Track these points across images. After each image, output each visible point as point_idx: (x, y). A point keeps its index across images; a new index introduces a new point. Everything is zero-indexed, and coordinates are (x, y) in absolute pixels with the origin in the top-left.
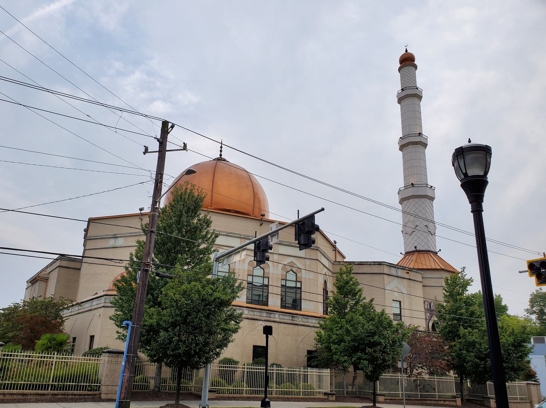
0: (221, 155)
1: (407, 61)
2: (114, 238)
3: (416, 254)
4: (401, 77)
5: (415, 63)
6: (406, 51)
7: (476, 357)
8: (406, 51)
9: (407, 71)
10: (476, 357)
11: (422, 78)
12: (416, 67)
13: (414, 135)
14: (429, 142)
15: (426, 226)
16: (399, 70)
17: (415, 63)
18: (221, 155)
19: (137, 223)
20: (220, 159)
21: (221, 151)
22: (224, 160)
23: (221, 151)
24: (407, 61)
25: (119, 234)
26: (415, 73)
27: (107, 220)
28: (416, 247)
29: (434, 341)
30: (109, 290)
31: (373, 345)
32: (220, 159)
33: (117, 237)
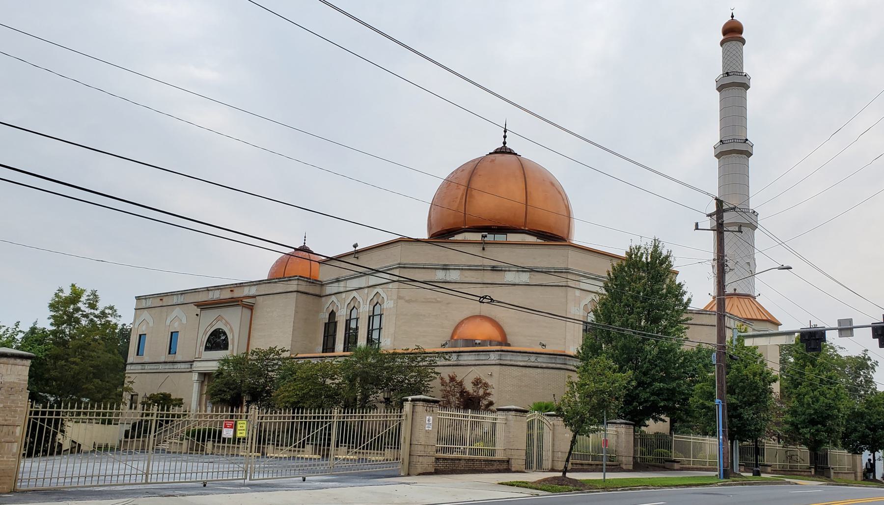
0: (505, 143)
1: (733, 32)
2: (443, 269)
3: (735, 297)
4: (723, 53)
5: (743, 36)
6: (732, 16)
7: (867, 427)
8: (732, 16)
9: (734, 48)
10: (867, 427)
11: (752, 61)
12: (743, 41)
13: (734, 141)
14: (755, 151)
15: (748, 263)
16: (722, 43)
17: (743, 36)
18: (505, 143)
19: (604, 268)
20: (504, 151)
21: (505, 137)
22: (511, 152)
23: (505, 137)
24: (733, 32)
25: (452, 265)
26: (742, 49)
27: (456, 245)
28: (735, 290)
29: (87, 398)
30: (443, 346)
31: (829, 417)
32: (504, 151)
33: (449, 269)
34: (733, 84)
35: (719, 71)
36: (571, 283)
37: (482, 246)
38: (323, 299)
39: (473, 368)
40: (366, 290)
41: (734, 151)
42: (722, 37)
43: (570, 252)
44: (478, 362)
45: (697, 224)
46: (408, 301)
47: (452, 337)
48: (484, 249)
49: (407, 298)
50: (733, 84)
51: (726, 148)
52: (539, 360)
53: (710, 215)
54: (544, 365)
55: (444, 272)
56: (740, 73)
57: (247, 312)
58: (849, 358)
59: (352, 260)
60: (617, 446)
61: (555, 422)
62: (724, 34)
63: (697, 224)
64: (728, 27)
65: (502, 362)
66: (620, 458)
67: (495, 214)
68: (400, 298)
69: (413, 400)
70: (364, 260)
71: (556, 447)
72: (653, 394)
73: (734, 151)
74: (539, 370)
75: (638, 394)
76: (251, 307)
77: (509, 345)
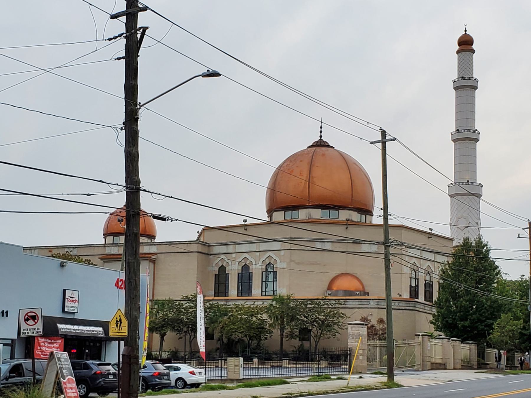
0: (321, 137)
1: (466, 44)
6: (466, 31)
8: (466, 31)
12: (473, 51)
14: (481, 137)
15: (477, 223)
16: (458, 52)
18: (321, 137)
20: (321, 144)
24: (466, 44)
32: (321, 144)
34: (466, 85)
35: (456, 77)
36: (404, 253)
37: (346, 226)
38: (211, 257)
39: (357, 310)
40: (258, 254)
41: (466, 138)
42: (457, 47)
43: (403, 231)
44: (360, 306)
45: (519, 235)
46: (298, 264)
47: (329, 288)
48: (347, 228)
49: (297, 262)
50: (466, 85)
51: (461, 135)
52: (401, 305)
53: (145, 9)
54: (403, 308)
55: (321, 243)
56: (471, 78)
57: (152, 265)
58: (511, 281)
59: (242, 230)
60: (470, 356)
61: (455, 344)
62: (459, 45)
63: (519, 235)
64: (464, 39)
65: (379, 307)
66: (472, 362)
67: (319, 193)
68: (291, 261)
69: (422, 335)
70: (250, 231)
71: (455, 357)
72: (486, 326)
73: (466, 138)
74: (401, 311)
75: (477, 327)
76: (154, 262)
77: (368, 294)
